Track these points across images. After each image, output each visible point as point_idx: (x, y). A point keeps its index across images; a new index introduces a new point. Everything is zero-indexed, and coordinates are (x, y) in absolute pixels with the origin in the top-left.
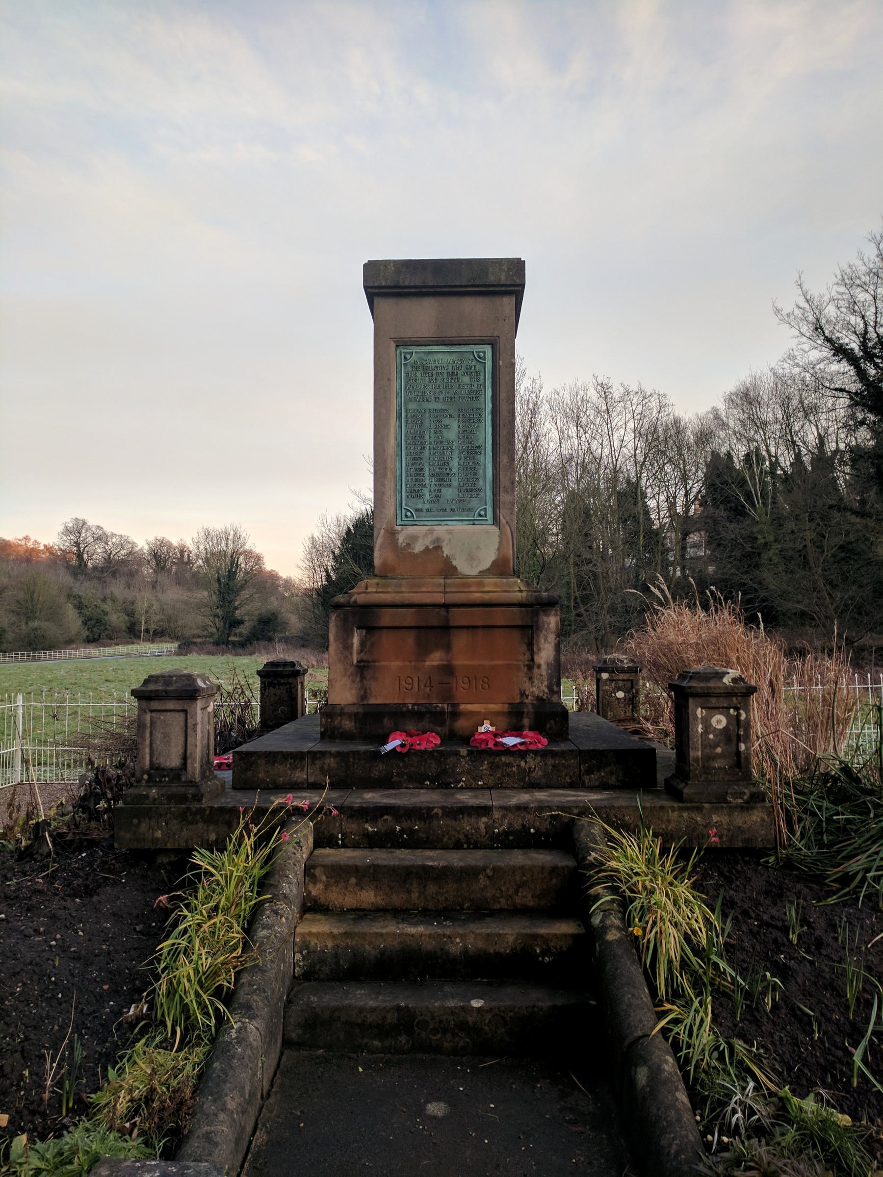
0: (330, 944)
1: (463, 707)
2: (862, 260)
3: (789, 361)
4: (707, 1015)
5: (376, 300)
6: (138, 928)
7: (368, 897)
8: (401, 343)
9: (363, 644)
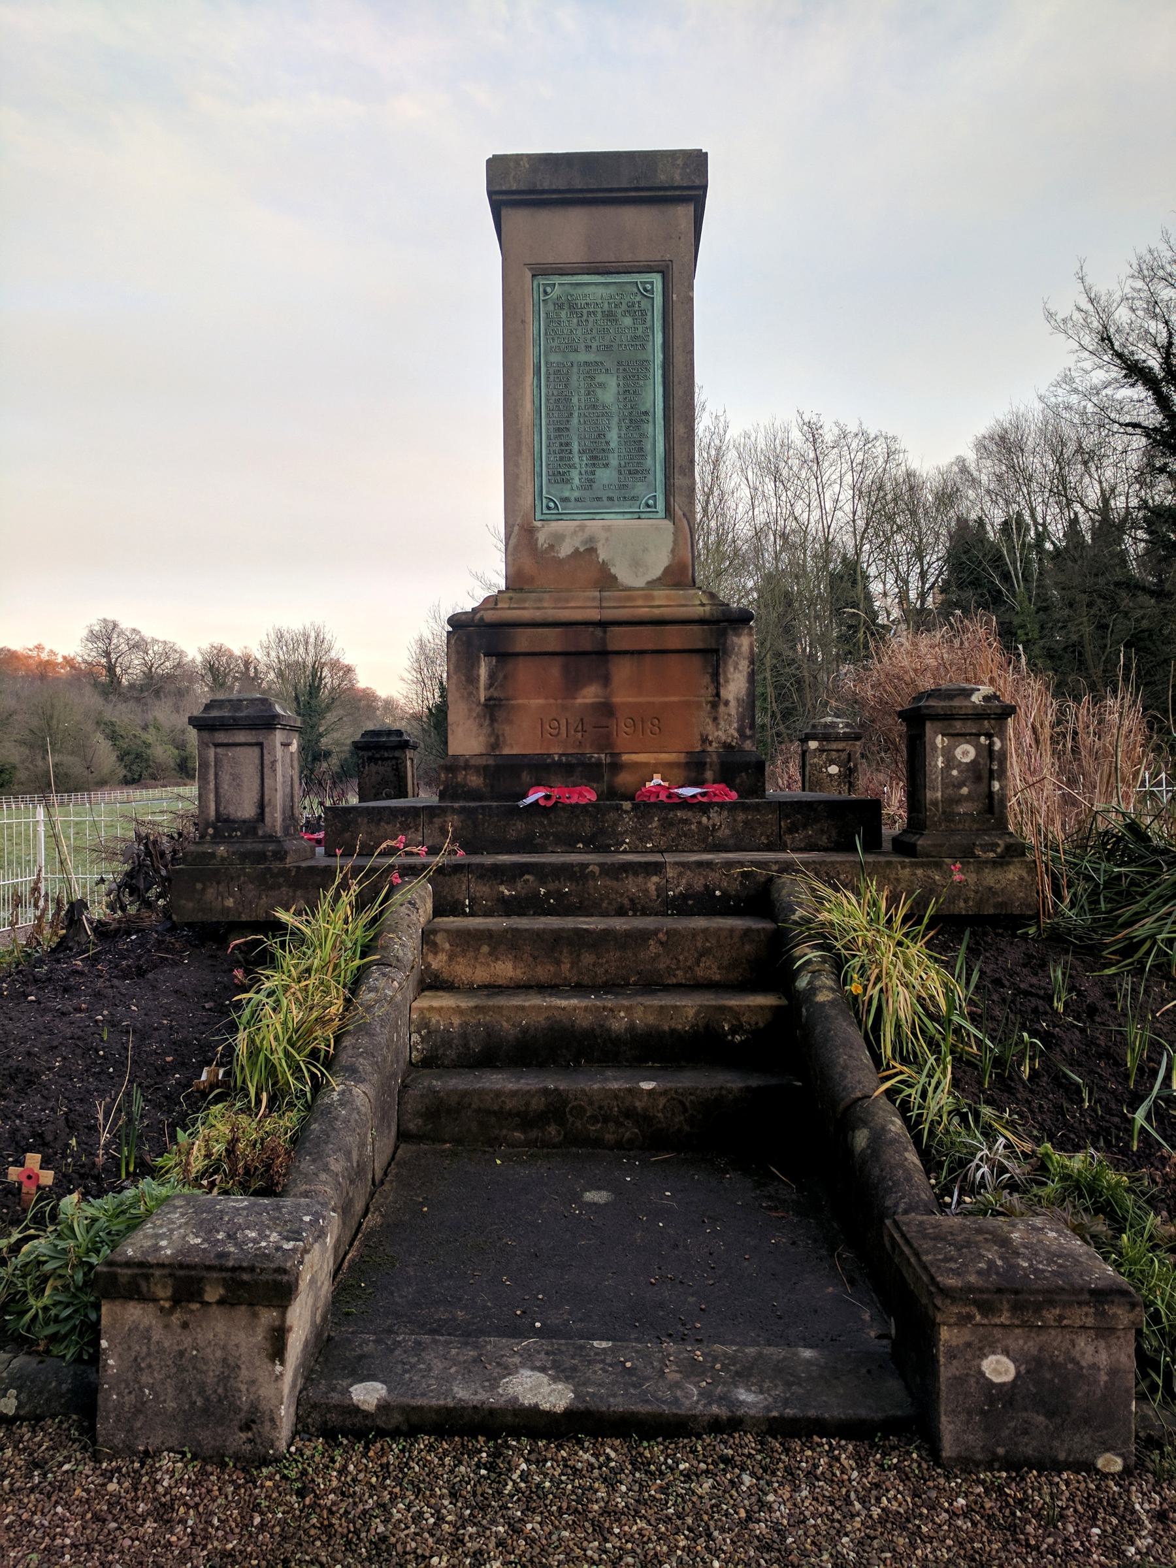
0: (456, 1021)
1: (625, 757)
2: (1168, 242)
3: (1064, 386)
4: (945, 1077)
5: (505, 212)
6: (207, 1006)
7: (506, 969)
8: (540, 271)
9: (492, 676)
